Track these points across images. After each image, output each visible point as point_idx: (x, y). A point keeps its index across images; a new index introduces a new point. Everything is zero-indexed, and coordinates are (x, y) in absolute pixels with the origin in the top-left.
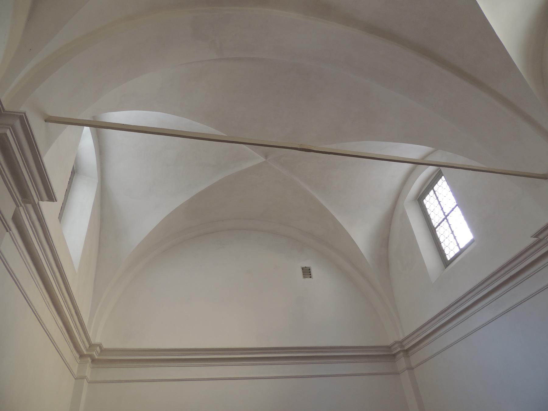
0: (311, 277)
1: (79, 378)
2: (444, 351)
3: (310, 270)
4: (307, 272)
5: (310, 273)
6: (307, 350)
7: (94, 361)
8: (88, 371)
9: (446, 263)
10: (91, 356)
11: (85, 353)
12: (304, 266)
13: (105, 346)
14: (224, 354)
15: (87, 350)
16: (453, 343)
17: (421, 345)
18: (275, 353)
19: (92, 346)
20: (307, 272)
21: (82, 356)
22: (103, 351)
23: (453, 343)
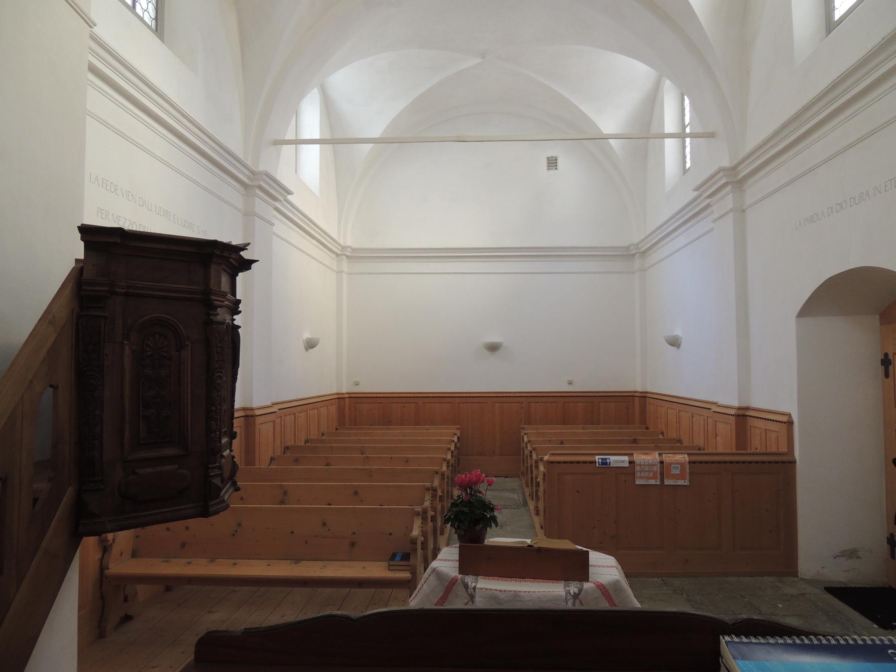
0: (556, 169)
1: (339, 272)
2: (775, 192)
3: (556, 160)
4: (552, 163)
5: (555, 161)
6: (537, 250)
7: (347, 257)
8: (345, 266)
9: (830, 25)
10: (344, 255)
11: (339, 253)
12: (550, 155)
13: (354, 246)
14: (456, 253)
15: (341, 251)
16: (123, 134)
17: (655, 248)
18: (528, 252)
19: (344, 248)
20: (552, 163)
21: (337, 255)
22: (354, 250)
23: (123, 134)
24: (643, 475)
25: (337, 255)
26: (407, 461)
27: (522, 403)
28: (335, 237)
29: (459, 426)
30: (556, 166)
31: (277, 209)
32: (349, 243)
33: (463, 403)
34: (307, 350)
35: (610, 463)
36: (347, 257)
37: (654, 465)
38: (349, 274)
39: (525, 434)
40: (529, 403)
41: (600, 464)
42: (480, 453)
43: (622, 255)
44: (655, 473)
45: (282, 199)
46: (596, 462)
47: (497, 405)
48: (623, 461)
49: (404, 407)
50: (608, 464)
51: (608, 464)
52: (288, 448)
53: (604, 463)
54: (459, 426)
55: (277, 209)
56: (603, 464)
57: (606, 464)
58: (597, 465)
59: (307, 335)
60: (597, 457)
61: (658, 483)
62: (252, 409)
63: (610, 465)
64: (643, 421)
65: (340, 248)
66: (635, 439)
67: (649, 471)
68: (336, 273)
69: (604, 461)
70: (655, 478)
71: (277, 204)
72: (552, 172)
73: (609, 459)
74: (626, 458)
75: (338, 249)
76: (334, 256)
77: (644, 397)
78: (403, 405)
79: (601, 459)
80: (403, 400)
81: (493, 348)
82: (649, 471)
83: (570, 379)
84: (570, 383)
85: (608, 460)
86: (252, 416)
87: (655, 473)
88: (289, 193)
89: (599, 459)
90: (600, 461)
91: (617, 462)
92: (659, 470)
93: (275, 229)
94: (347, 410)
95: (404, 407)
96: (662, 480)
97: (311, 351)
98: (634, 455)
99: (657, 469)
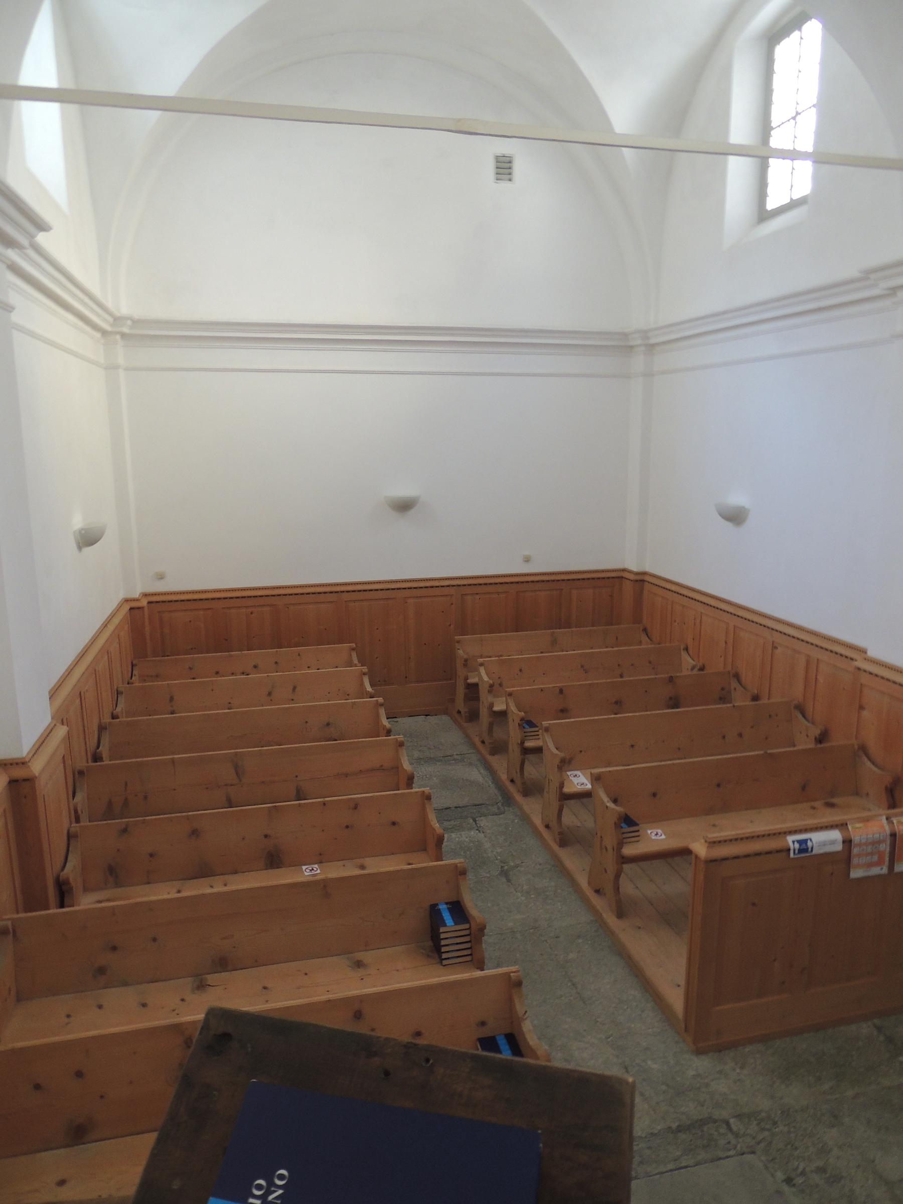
0: (510, 180)
1: (111, 368)
3: (510, 162)
5: (508, 165)
7: (123, 335)
11: (107, 327)
15: (111, 325)
21: (104, 333)
22: (136, 322)
24: (863, 860)
25: (104, 333)
26: (356, 808)
27: (451, 596)
28: (96, 290)
29: (353, 645)
30: (510, 174)
31: (14, 269)
32: (125, 309)
33: (354, 601)
34: (80, 548)
35: (812, 848)
36: (123, 335)
37: (879, 842)
38: (127, 369)
39: (481, 665)
40: (462, 594)
41: (797, 852)
42: (385, 681)
43: (613, 346)
44: (881, 855)
45: (24, 242)
46: (789, 850)
47: (411, 601)
48: (833, 842)
49: (252, 613)
50: (810, 850)
51: (810, 850)
52: (81, 773)
53: (804, 846)
54: (353, 645)
55: (14, 269)
56: (801, 851)
57: (806, 850)
58: (792, 855)
59: (78, 522)
60: (790, 839)
61: (885, 870)
62: (23, 763)
63: (812, 851)
64: (637, 618)
65: (111, 319)
66: (672, 677)
67: (872, 854)
68: (106, 368)
69: (804, 846)
70: (879, 863)
71: (12, 254)
72: (504, 185)
73: (811, 840)
74: (835, 835)
75: (105, 320)
76: (98, 335)
77: (641, 580)
78: (250, 610)
79: (799, 841)
80: (250, 602)
81: (404, 506)
82: (872, 854)
83: (527, 553)
84: (527, 560)
85: (809, 844)
86: (25, 780)
87: (881, 855)
88: (42, 226)
89: (793, 842)
90: (797, 846)
91: (824, 844)
92: (888, 849)
93: (15, 317)
94: (147, 629)
95: (252, 613)
96: (891, 867)
97: (87, 550)
98: (850, 827)
99: (885, 847)
